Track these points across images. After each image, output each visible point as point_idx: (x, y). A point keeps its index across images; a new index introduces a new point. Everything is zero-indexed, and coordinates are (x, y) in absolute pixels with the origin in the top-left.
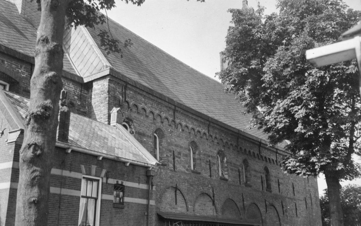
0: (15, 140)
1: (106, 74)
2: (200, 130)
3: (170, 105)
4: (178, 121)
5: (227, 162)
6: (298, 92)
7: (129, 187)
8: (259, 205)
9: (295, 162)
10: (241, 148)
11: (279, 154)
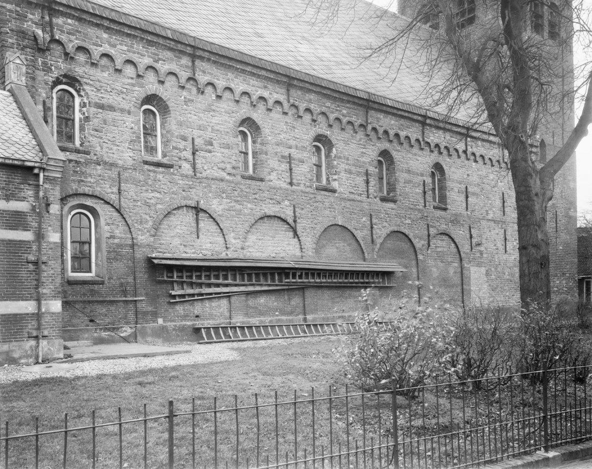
2: (266, 94)
3: (179, 45)
4: (203, 79)
11: (472, 137)
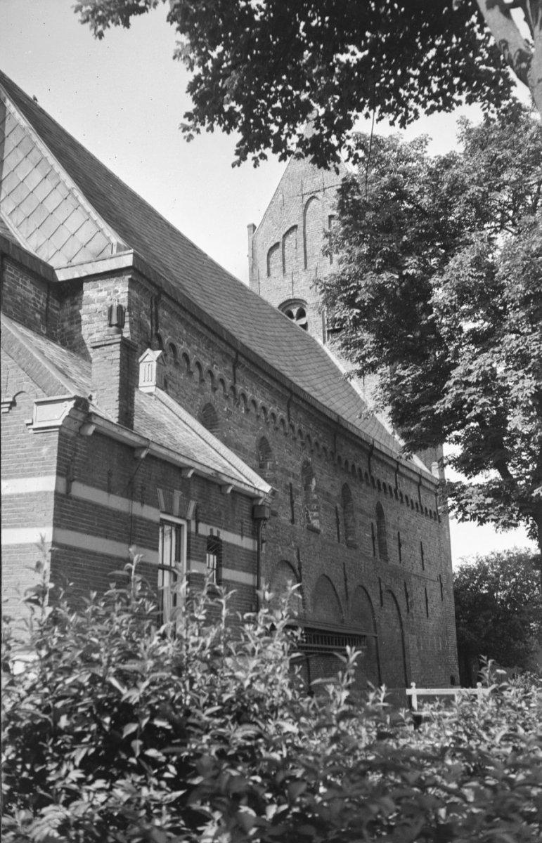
0: (60, 423)
1: (124, 265)
3: (228, 348)
4: (239, 388)
5: (317, 490)
6: (520, 340)
7: (228, 544)
8: (370, 590)
9: (482, 497)
10: (339, 457)
11: (402, 475)
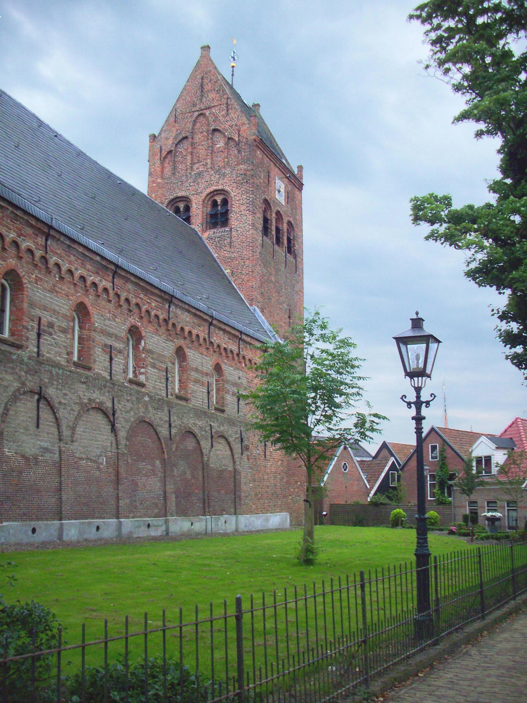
4: (53, 260)
11: (244, 341)
